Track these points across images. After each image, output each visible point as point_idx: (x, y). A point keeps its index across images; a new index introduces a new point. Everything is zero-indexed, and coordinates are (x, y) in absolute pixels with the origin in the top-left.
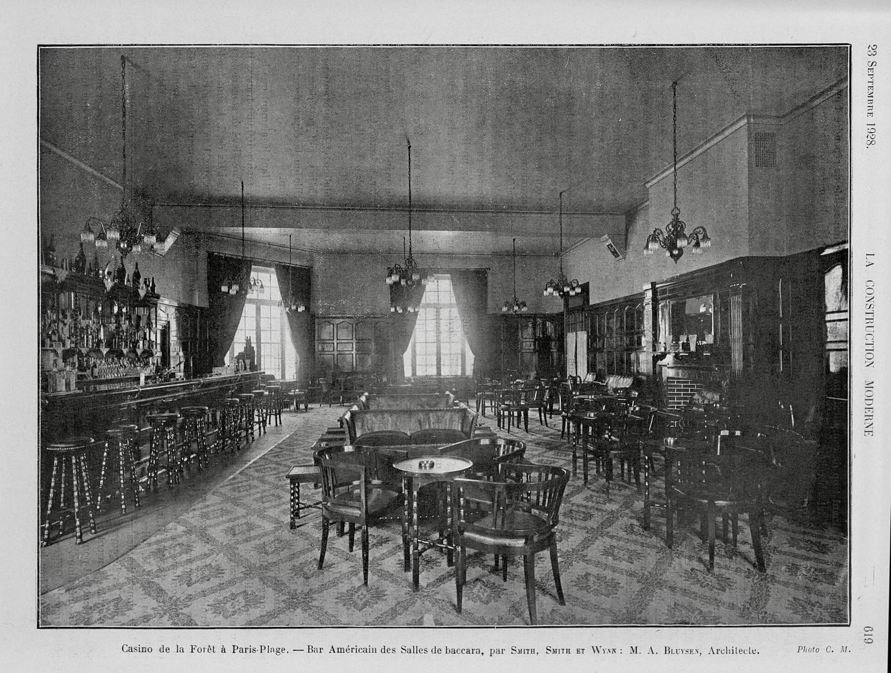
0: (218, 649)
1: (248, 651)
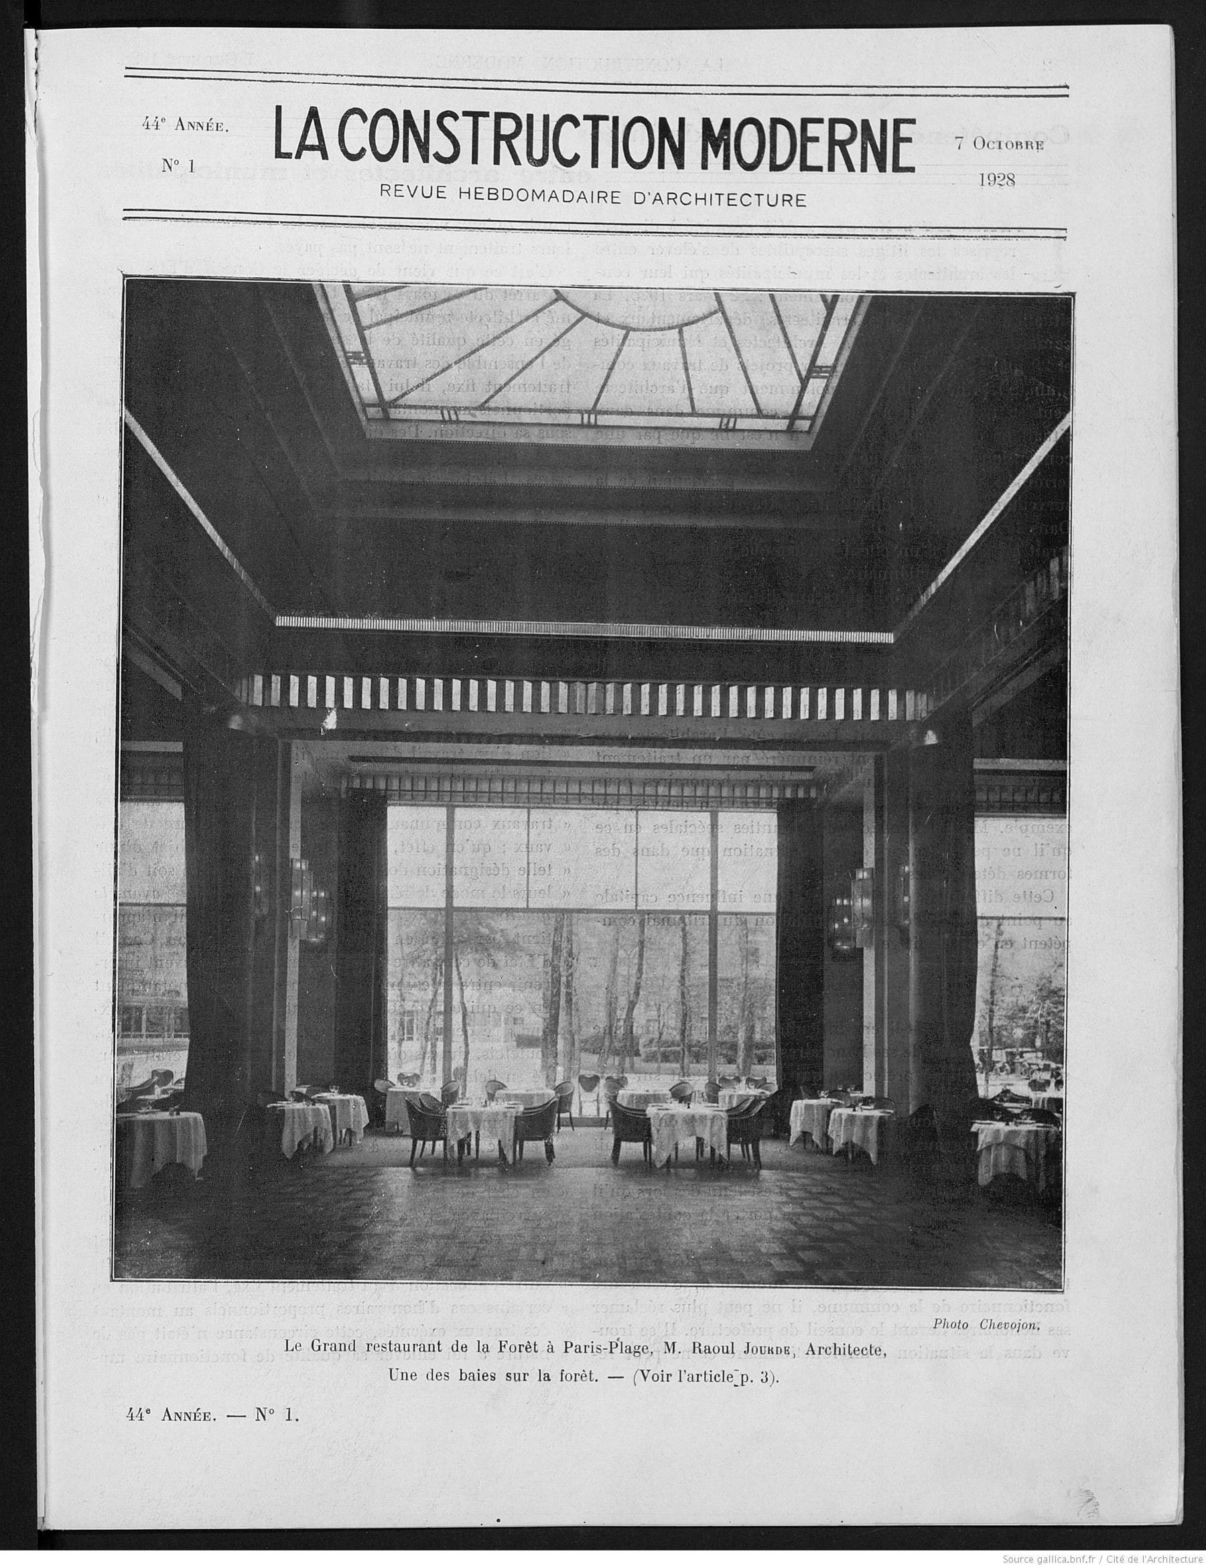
0: (542, 1346)
1: (523, 1349)
